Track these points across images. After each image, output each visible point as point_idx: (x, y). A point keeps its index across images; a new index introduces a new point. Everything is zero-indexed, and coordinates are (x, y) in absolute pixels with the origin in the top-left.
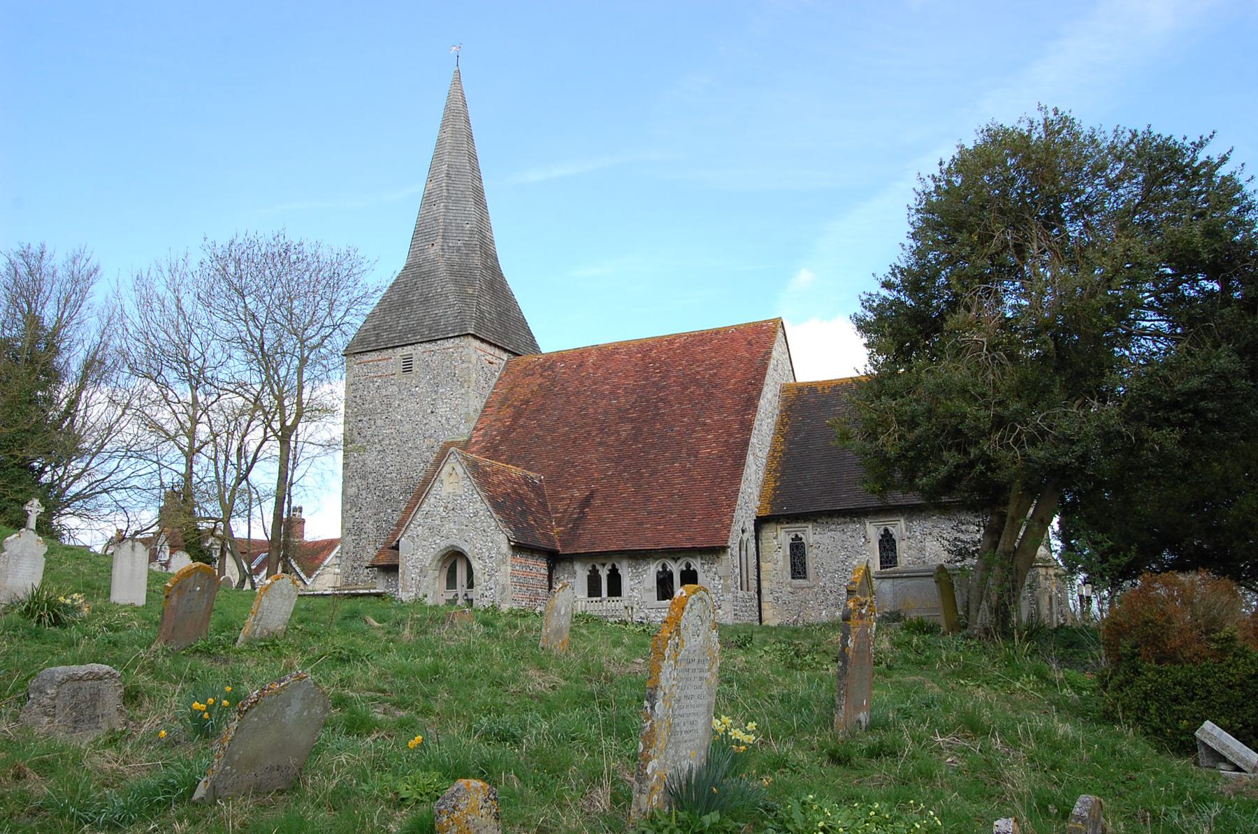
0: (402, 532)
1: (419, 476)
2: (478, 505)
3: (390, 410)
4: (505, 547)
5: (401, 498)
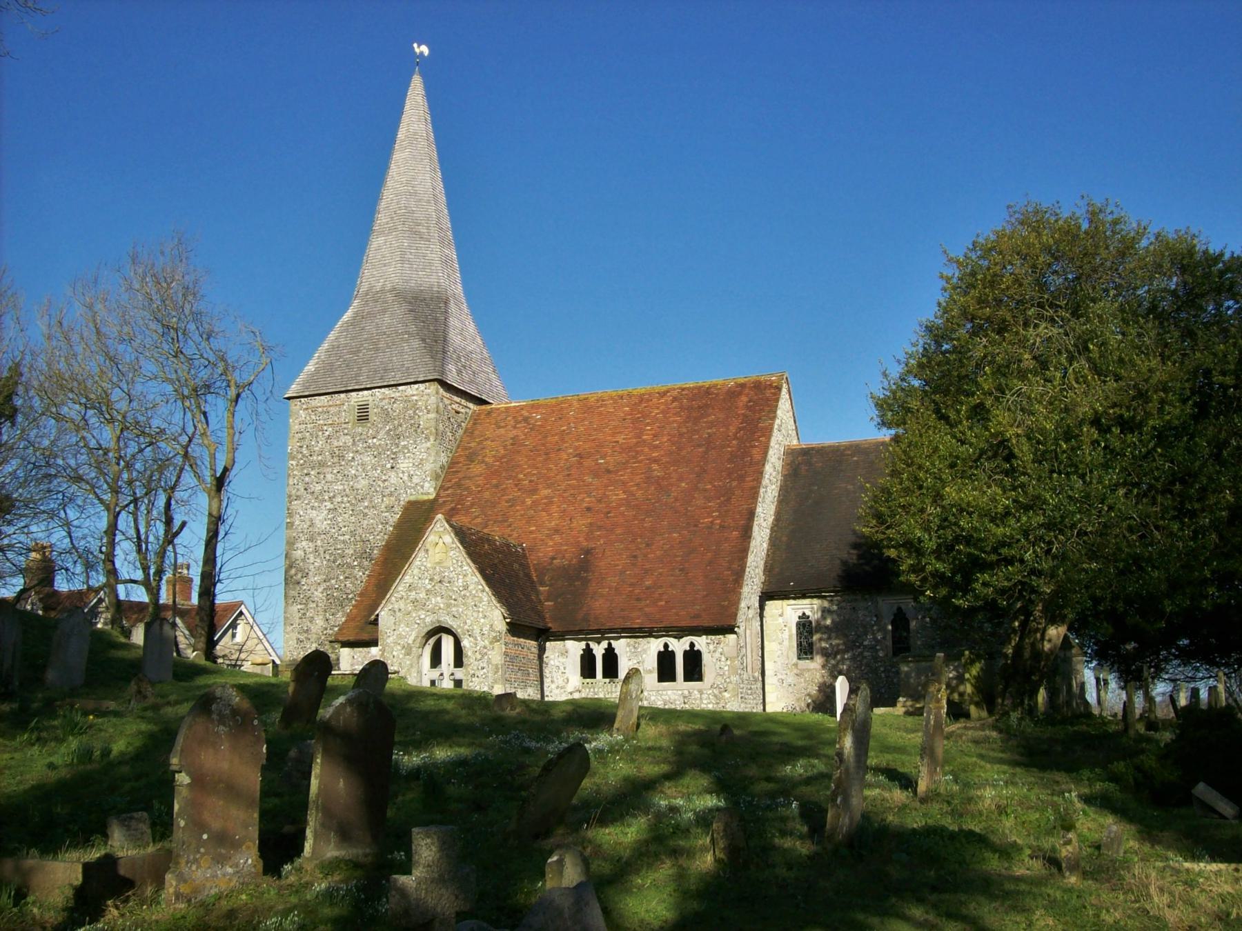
0: (382, 605)
2: (469, 577)
3: (343, 463)
4: (501, 626)
5: (356, 563)
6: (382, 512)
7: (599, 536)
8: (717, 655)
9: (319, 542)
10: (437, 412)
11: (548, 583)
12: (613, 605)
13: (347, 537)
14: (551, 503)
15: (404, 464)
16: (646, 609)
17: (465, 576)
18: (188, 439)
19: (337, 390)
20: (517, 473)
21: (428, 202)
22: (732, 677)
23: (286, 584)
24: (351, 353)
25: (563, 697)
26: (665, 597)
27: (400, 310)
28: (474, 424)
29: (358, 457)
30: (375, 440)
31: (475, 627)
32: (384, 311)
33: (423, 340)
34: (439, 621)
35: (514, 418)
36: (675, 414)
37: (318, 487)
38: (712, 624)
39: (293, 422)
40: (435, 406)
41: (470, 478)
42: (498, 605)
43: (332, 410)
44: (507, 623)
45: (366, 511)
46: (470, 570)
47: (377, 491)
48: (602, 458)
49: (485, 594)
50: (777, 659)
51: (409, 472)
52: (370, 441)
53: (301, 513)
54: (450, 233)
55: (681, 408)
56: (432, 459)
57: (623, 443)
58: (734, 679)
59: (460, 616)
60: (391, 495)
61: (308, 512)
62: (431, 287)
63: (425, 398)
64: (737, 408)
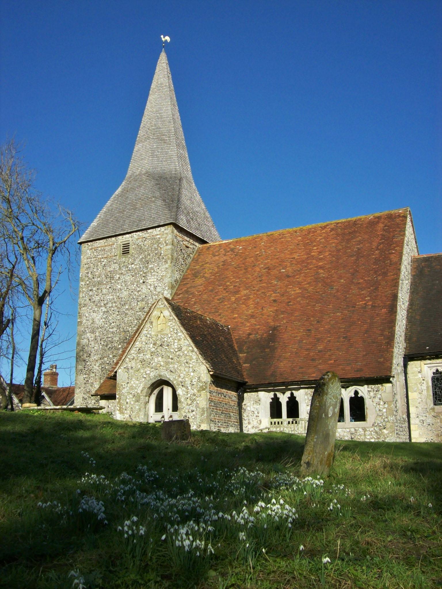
1: (131, 330)
3: (113, 281)
4: (206, 377)
5: (120, 346)
6: (137, 312)
7: (283, 318)
8: (377, 400)
9: (97, 333)
10: (172, 244)
11: (245, 351)
12: (294, 365)
13: (115, 329)
14: (249, 299)
15: (151, 280)
16: (319, 367)
17: (179, 340)
18: (12, 266)
19: (110, 235)
20: (226, 282)
21: (170, 122)
22: (389, 418)
23: (76, 361)
24: (120, 212)
25: (252, 431)
26: (334, 357)
27: (150, 184)
28: (199, 255)
29: (122, 277)
30: (133, 265)
31: (187, 379)
32: (140, 186)
33: (164, 201)
34: (160, 376)
35: (224, 249)
36: (333, 238)
37: (98, 298)
38: (372, 376)
39: (83, 258)
40: (171, 240)
41: (194, 287)
42: (204, 361)
43: (107, 248)
44: (211, 375)
45: (127, 311)
46: (183, 336)
47: (134, 298)
48: (283, 269)
49: (194, 353)
50: (418, 405)
51: (154, 285)
52: (130, 266)
53: (87, 315)
54: (184, 142)
55: (338, 235)
56: (169, 275)
57: (297, 259)
58: (391, 418)
59: (176, 371)
60: (143, 300)
61: (91, 314)
62: (171, 171)
63: (165, 236)
64: (376, 231)
